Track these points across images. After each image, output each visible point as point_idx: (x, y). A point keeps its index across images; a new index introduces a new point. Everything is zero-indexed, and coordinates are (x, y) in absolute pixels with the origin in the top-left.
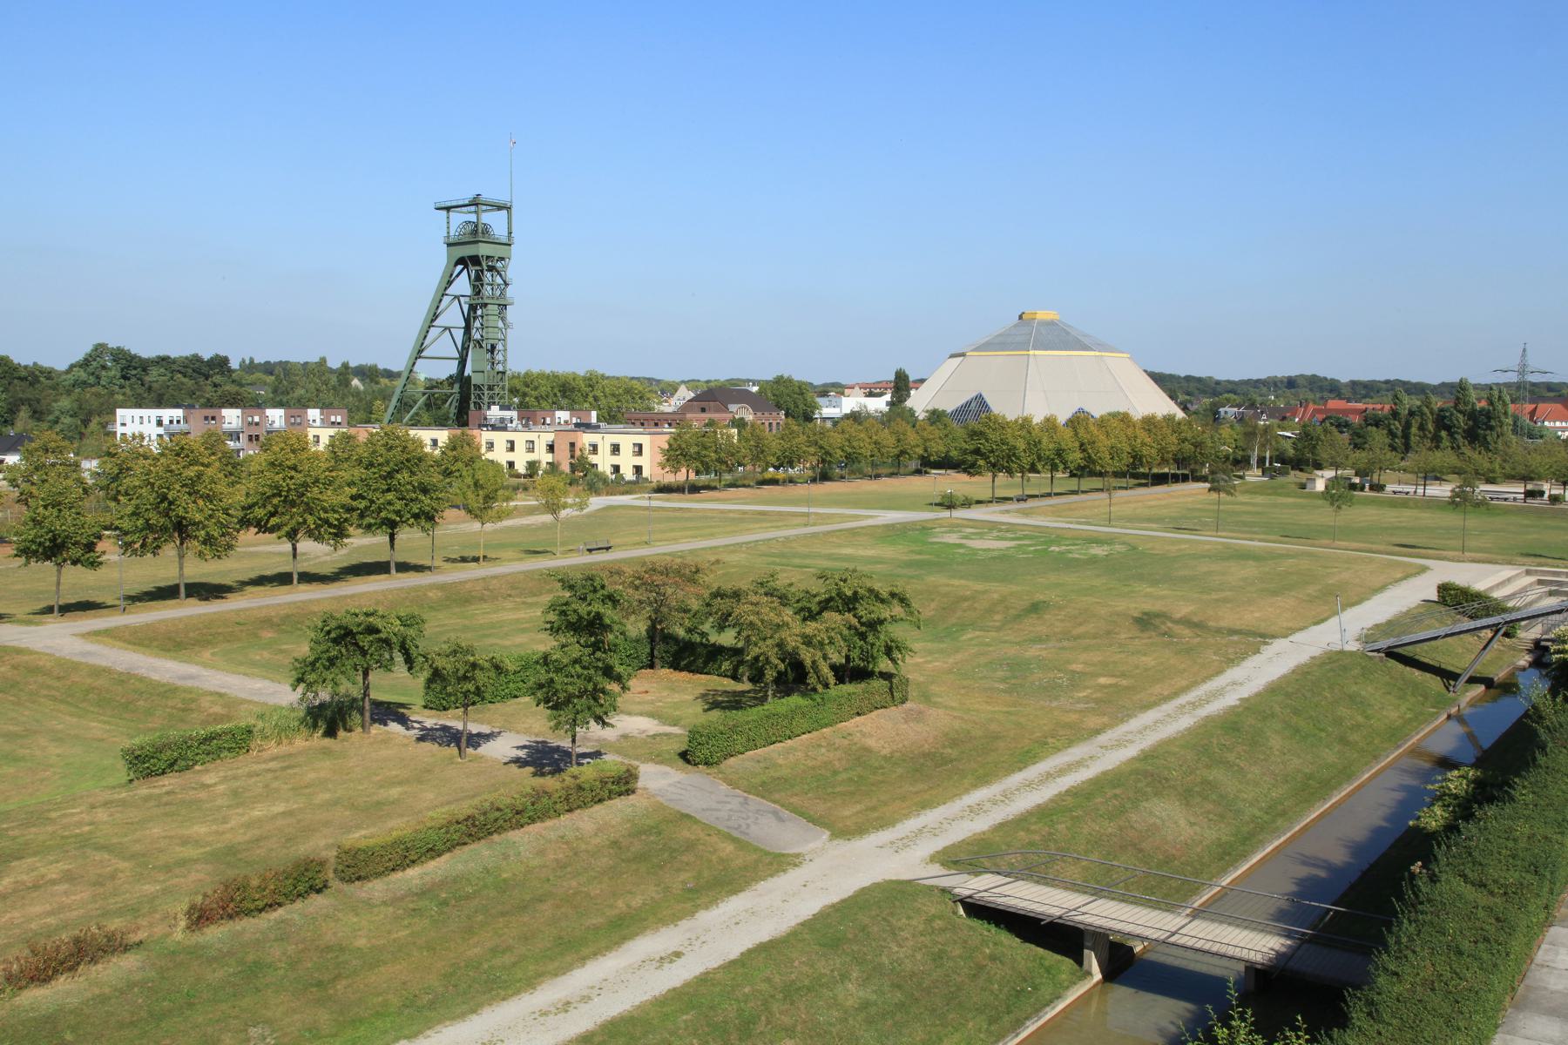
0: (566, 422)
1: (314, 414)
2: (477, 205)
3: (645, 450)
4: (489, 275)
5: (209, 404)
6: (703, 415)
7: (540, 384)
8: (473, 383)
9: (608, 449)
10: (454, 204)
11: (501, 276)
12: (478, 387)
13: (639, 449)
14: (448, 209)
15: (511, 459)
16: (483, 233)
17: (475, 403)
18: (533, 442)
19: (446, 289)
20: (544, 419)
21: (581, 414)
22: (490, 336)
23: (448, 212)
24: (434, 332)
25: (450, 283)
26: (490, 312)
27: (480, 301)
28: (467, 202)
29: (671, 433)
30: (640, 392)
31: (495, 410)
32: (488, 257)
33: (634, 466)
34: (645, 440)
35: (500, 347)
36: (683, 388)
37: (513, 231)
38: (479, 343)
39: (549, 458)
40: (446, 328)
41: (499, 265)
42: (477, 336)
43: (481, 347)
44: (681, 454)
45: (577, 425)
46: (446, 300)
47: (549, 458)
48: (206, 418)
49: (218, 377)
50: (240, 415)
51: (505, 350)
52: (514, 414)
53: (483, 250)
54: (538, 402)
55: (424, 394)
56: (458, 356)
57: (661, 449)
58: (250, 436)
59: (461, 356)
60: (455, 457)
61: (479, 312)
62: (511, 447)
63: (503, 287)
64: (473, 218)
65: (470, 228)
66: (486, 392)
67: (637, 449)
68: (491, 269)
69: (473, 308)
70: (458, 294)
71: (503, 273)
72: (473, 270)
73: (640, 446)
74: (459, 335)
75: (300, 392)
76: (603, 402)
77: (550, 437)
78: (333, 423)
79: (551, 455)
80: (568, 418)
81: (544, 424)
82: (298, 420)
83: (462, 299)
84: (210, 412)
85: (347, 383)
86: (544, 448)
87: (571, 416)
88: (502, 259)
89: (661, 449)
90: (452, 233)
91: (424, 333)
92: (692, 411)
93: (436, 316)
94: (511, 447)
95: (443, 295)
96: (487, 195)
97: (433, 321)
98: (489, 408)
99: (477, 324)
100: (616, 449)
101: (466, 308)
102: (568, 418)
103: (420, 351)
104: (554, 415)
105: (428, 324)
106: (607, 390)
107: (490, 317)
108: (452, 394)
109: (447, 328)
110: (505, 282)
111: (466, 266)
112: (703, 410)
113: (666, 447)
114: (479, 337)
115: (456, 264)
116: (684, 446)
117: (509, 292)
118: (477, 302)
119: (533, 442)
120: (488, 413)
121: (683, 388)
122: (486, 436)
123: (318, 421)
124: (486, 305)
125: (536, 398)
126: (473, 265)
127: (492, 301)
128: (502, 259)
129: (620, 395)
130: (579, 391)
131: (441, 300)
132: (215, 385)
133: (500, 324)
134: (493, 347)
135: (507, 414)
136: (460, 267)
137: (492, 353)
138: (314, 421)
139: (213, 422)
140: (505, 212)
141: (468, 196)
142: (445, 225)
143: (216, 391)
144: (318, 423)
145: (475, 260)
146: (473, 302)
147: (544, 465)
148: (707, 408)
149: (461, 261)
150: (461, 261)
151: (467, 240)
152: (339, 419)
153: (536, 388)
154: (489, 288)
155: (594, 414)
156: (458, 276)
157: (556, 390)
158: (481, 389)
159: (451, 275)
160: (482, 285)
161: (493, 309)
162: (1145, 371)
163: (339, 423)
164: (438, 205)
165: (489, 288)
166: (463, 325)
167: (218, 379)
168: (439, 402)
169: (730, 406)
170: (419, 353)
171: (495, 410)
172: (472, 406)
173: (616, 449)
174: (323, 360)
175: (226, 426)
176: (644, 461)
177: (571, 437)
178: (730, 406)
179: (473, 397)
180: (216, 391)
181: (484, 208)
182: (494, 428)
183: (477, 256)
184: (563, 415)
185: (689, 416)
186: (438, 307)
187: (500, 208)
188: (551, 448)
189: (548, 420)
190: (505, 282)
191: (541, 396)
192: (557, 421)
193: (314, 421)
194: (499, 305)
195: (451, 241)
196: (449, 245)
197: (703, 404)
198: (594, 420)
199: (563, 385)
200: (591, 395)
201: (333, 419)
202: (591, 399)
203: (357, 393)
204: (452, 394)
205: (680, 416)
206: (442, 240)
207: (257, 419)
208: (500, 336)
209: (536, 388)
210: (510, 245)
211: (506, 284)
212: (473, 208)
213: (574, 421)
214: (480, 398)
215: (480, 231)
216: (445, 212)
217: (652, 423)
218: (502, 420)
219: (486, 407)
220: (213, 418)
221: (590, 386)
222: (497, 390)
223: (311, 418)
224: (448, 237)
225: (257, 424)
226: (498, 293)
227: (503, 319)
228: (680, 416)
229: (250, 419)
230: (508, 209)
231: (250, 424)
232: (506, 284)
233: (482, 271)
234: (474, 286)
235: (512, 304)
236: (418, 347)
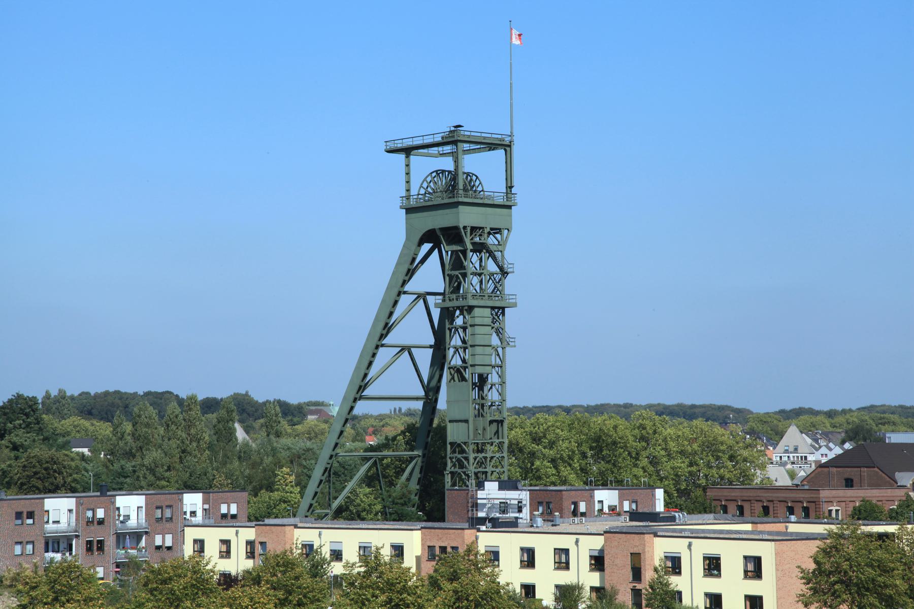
0: (612, 509)
1: (193, 501)
2: (455, 143)
3: (768, 568)
4: (475, 258)
5: (26, 487)
6: (850, 493)
7: (558, 437)
8: (449, 439)
9: (699, 566)
10: (418, 142)
11: (495, 259)
12: (458, 447)
13: (754, 567)
14: (407, 151)
15: (528, 581)
16: (465, 190)
17: (452, 473)
18: (566, 551)
19: (404, 283)
20: (576, 504)
21: (640, 494)
22: (478, 360)
23: (408, 157)
24: (384, 355)
25: (411, 273)
26: (478, 321)
27: (461, 303)
28: (438, 139)
29: (821, 537)
30: (730, 447)
31: (491, 491)
32: (473, 229)
33: (747, 597)
34: (765, 551)
35: (494, 378)
36: (793, 436)
37: (515, 182)
38: (459, 373)
39: (593, 579)
40: (403, 349)
41: (491, 241)
42: (457, 361)
43: (463, 379)
44: (841, 582)
45: (634, 516)
46: (405, 300)
47: (593, 579)
48: (19, 515)
49: (21, 432)
50: (73, 507)
51: (503, 383)
52: (524, 496)
53: (466, 217)
54: (556, 467)
55: (366, 459)
56: (421, 393)
57: (803, 571)
58: (89, 543)
59: (427, 389)
60: (456, 592)
61: (459, 321)
62: (529, 559)
63: (498, 277)
64: (447, 164)
65: (443, 182)
66: (472, 456)
67: (751, 567)
68: (479, 248)
69: (447, 314)
70: (422, 290)
71: (498, 254)
72: (448, 249)
73: (757, 561)
74: (425, 358)
75: (153, 455)
76: (667, 467)
77: (597, 543)
78: (224, 516)
79: (596, 575)
80: (615, 502)
81: (575, 513)
82: (168, 513)
83: (431, 300)
84: (24, 503)
85: (226, 435)
86: (585, 562)
87: (621, 499)
88: (496, 231)
89: (803, 571)
90: (414, 192)
91: (368, 358)
92: (828, 485)
93: (387, 329)
94: (529, 559)
95: (399, 294)
96: (474, 126)
97: (382, 336)
98: (480, 486)
99: (456, 341)
100: (713, 566)
101: (436, 314)
102: (615, 502)
103: (362, 388)
104: (592, 497)
105: (375, 341)
106: (672, 444)
107: (478, 330)
108: (412, 458)
109: (405, 349)
110: (501, 268)
111: (437, 245)
112: (849, 483)
113: (812, 566)
114: (460, 363)
115: (421, 243)
116: (845, 566)
117: (510, 285)
118: (456, 303)
119: (566, 551)
120: (480, 494)
121: (793, 436)
122: (486, 540)
123: (200, 513)
124: (471, 309)
125: (553, 461)
126: (449, 243)
127: (482, 303)
128: (496, 231)
129: (695, 453)
130: (625, 447)
131: (396, 302)
132: (15, 448)
133: (495, 340)
134: (483, 379)
135: (512, 496)
136: (427, 247)
137: (481, 389)
138: (193, 513)
139: (30, 521)
140: (501, 153)
141: (439, 128)
142: (403, 178)
143: (17, 458)
144: (199, 518)
145: (453, 234)
146: (448, 304)
147: (587, 592)
148: (856, 480)
149: (430, 236)
150: (430, 236)
151: (439, 201)
152: (234, 510)
153: (552, 445)
154: (475, 280)
155: (660, 493)
156: (423, 261)
157: (585, 448)
158: (463, 451)
159: (414, 260)
160: (464, 275)
161: (482, 315)
162: (463, 126)
163: (234, 517)
164: (391, 146)
165: (475, 280)
166: (432, 341)
167: (19, 436)
168: (391, 472)
169: (898, 475)
170: (360, 389)
171: (491, 491)
172: (448, 479)
173: (713, 566)
174: (542, 600)
175: (50, 527)
176: (765, 588)
177: (633, 543)
178: (898, 475)
179: (449, 464)
180: (17, 458)
181: (466, 146)
182: (496, 524)
183: (456, 228)
184: (606, 497)
185: (825, 494)
186: (391, 314)
187: (492, 146)
188: (598, 562)
189: (582, 507)
190: (501, 268)
191: (562, 458)
192: (597, 507)
193: (193, 513)
194: (493, 308)
195: (413, 203)
196: (409, 210)
197: (849, 472)
198: (660, 507)
199: (597, 439)
200: (644, 454)
201: (224, 509)
202: (644, 462)
203: (244, 454)
204: (412, 458)
205: (807, 495)
206: (398, 203)
207: (100, 513)
208: (494, 360)
209: (552, 445)
210: (509, 207)
211: (504, 273)
212: (448, 149)
213: (626, 506)
214: (462, 466)
215: (461, 186)
216: (401, 157)
217: (758, 508)
218: (504, 507)
219: (472, 482)
220: (31, 515)
221: (642, 438)
222: (490, 450)
223: (188, 509)
224: (408, 198)
225: (101, 522)
226: (490, 286)
227: (499, 332)
228: (807, 495)
229: (89, 514)
230: (507, 147)
231: (90, 522)
232: (504, 273)
233: (464, 252)
234: (451, 277)
235: (514, 305)
236: (358, 382)
